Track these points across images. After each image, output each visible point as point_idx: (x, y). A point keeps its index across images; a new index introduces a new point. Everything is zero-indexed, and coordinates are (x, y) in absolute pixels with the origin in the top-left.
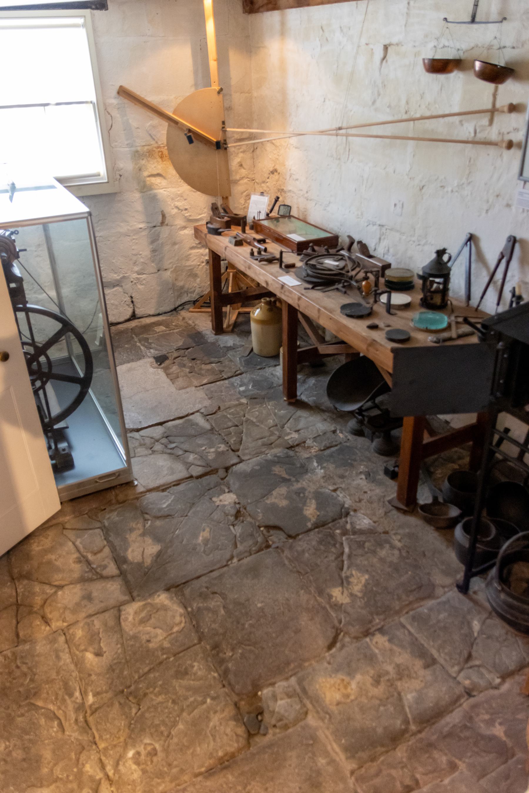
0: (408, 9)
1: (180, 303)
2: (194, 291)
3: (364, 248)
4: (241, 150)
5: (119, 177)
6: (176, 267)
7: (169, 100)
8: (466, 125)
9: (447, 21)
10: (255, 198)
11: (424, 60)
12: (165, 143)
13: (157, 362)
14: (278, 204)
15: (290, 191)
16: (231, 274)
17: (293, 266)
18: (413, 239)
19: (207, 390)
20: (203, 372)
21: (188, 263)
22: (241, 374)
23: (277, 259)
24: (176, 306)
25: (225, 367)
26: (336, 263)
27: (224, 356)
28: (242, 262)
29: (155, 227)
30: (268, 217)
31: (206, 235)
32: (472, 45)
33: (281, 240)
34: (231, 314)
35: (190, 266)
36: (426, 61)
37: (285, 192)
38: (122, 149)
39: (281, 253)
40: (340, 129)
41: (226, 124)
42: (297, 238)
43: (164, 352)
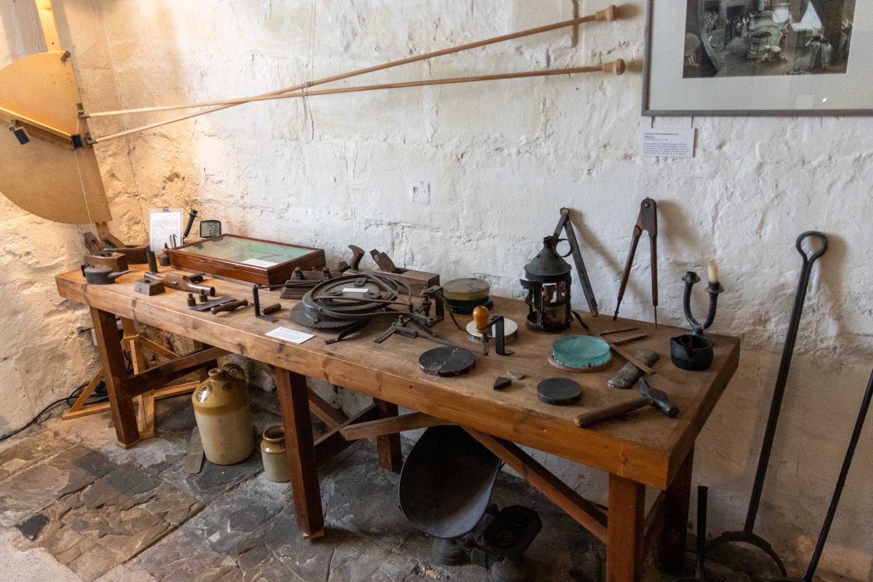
1: (42, 409)
2: (65, 382)
3: (383, 259)
4: (108, 153)
6: (24, 350)
10: (156, 218)
13: (26, 533)
14: (196, 224)
15: (209, 200)
16: (132, 342)
17: (277, 309)
18: (457, 234)
19: (149, 561)
20: (128, 527)
21: (46, 340)
22: (201, 509)
23: (245, 303)
24: (36, 415)
25: (165, 504)
27: (157, 483)
28: (177, 320)
30: (186, 245)
31: (84, 287)
34: (146, 409)
35: (50, 343)
37: (200, 204)
40: (310, 85)
43: (37, 510)
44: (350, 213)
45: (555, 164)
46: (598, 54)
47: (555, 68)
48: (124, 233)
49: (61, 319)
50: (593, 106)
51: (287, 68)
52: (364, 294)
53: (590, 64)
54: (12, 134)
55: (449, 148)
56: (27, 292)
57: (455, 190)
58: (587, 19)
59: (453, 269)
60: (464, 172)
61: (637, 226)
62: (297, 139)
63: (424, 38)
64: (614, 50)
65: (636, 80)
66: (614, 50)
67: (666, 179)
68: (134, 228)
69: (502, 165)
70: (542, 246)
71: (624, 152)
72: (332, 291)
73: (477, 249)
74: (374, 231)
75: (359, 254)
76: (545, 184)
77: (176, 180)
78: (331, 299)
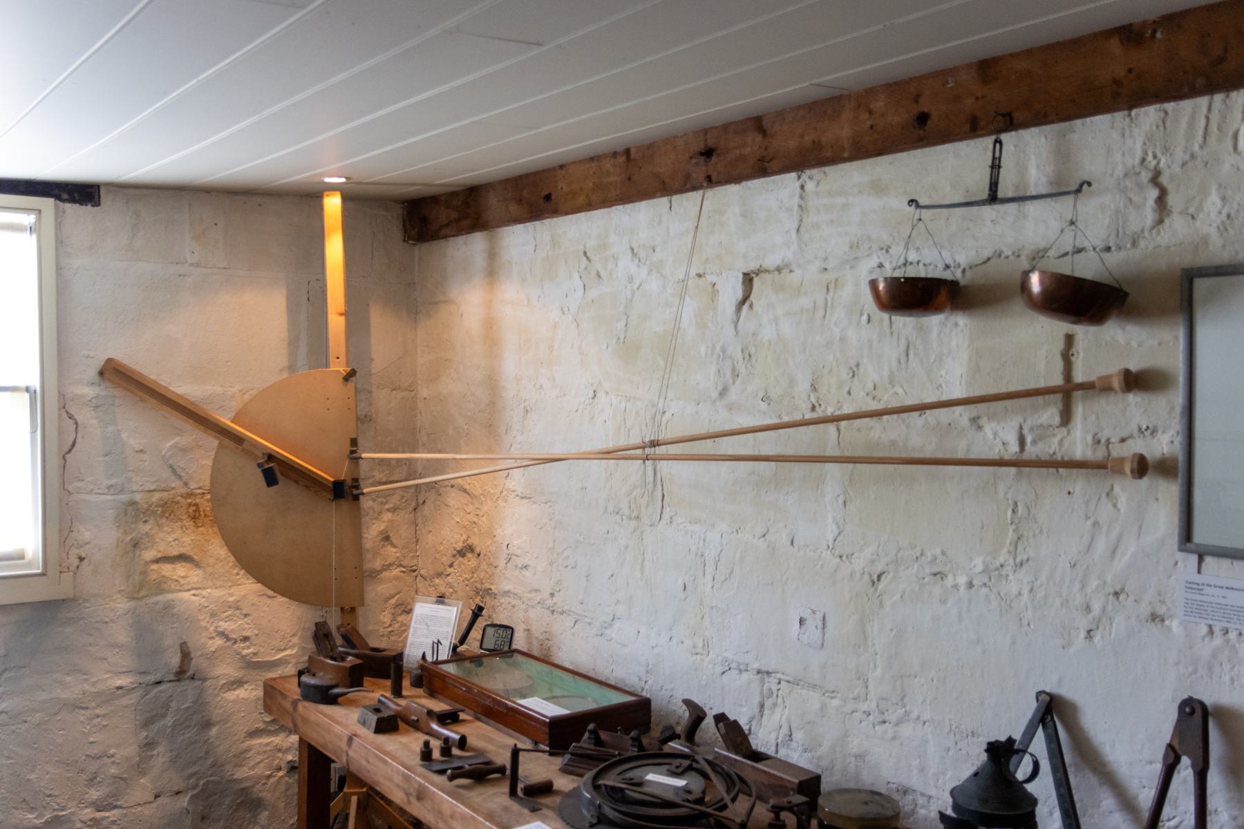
0: (801, 197)
3: (734, 733)
5: (76, 562)
6: (206, 784)
7: (222, 395)
8: (989, 428)
9: (918, 206)
10: (423, 609)
11: (873, 284)
12: (208, 483)
14: (481, 623)
16: (354, 799)
17: (545, 789)
18: (864, 707)
21: (240, 774)
23: (502, 770)
26: (680, 783)
28: (398, 779)
29: (159, 683)
30: (456, 656)
31: (295, 704)
32: (986, 253)
33: (502, 715)
35: (247, 778)
36: (881, 286)
37: (494, 596)
38: (93, 498)
39: (516, 753)
40: (654, 444)
41: (360, 441)
42: (544, 707)
44: (700, 645)
45: (1030, 612)
46: (1103, 441)
47: (1033, 457)
48: (376, 631)
49: (268, 744)
50: (1096, 524)
51: (637, 414)
52: (677, 788)
53: (1090, 455)
54: (259, 471)
55: (859, 563)
56: (231, 696)
57: (864, 632)
58: (1087, 387)
59: (852, 767)
60: (881, 604)
61: (1170, 746)
62: (638, 517)
63: (833, 391)
64: (1131, 437)
65: (1168, 493)
66: (1131, 437)
67: (1227, 667)
68: (400, 619)
69: (943, 601)
70: (984, 757)
71: (1149, 609)
72: (629, 775)
73: (894, 738)
74: (736, 681)
75: (698, 715)
76: (1013, 643)
77: (469, 555)
78: (622, 790)
